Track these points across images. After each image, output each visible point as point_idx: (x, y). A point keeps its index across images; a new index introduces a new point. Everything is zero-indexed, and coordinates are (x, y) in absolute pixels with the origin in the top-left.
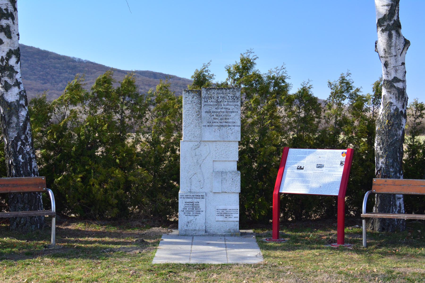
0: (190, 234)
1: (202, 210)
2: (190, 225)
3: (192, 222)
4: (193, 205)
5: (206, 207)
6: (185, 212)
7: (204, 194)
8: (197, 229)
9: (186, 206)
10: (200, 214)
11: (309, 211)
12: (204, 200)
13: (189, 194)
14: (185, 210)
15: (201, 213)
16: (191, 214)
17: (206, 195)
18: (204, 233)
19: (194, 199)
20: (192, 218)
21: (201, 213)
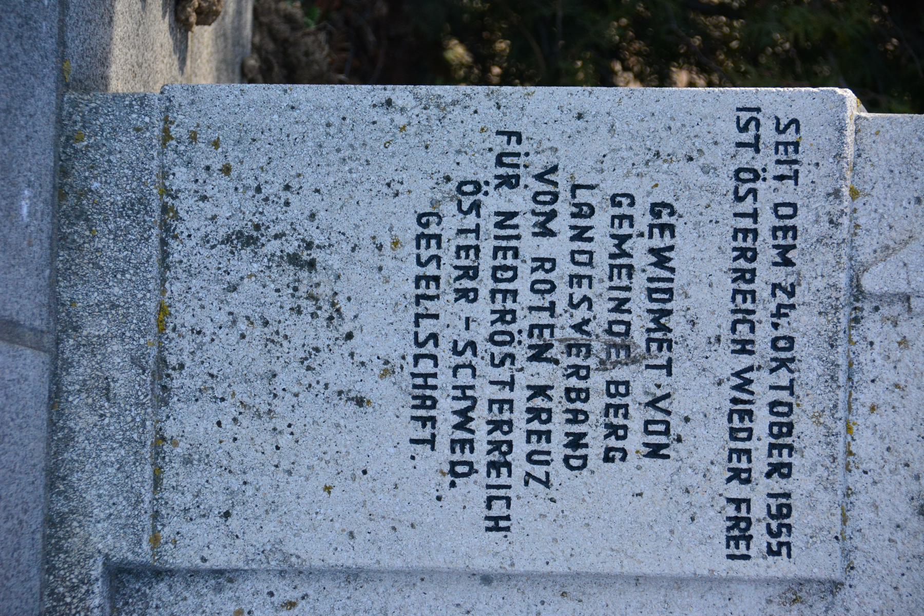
0: (83, 295)
1: (527, 504)
2: (261, 287)
3: (305, 331)
4: (620, 343)
5: (567, 585)
6: (495, 202)
7: (811, 559)
8: (189, 422)
9: (600, 223)
10: (457, 472)
11: (627, 389)
12: (712, 557)
13: (817, 272)
14: (518, 200)
15: (474, 489)
16: (449, 310)
17: (795, 591)
18: (103, 536)
19: (728, 363)
20: (384, 332)
21: (474, 489)
